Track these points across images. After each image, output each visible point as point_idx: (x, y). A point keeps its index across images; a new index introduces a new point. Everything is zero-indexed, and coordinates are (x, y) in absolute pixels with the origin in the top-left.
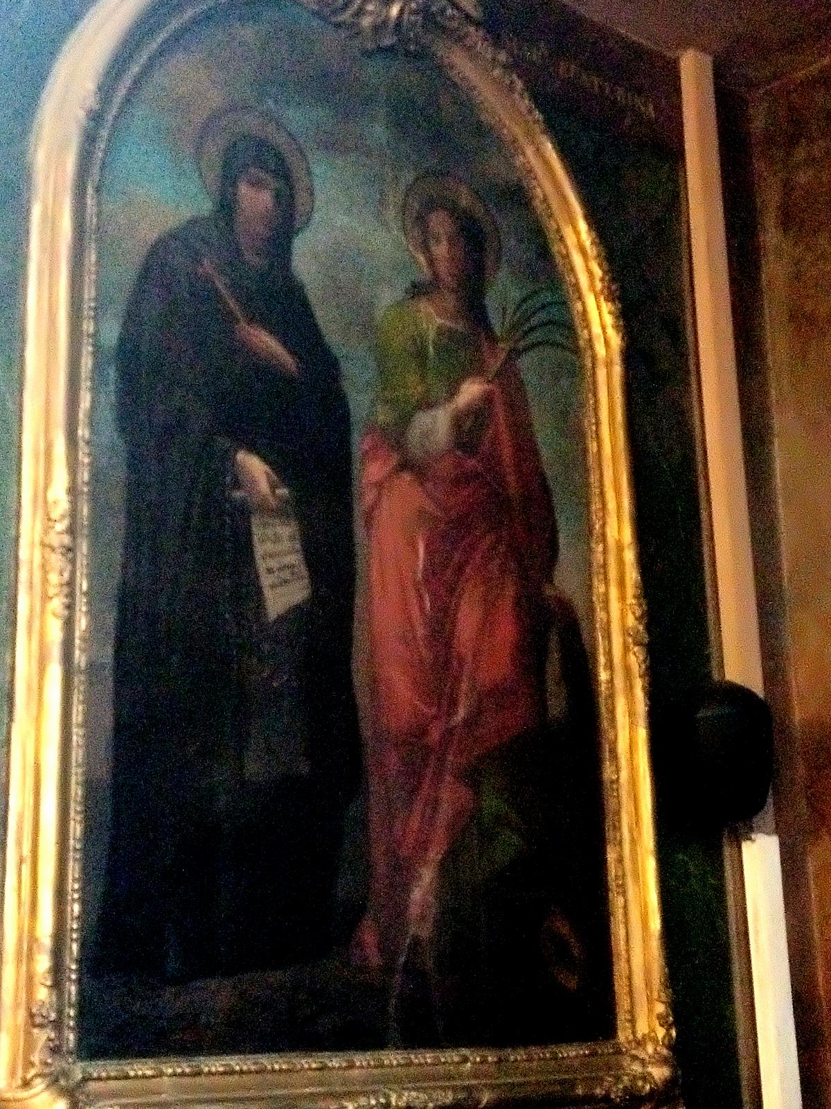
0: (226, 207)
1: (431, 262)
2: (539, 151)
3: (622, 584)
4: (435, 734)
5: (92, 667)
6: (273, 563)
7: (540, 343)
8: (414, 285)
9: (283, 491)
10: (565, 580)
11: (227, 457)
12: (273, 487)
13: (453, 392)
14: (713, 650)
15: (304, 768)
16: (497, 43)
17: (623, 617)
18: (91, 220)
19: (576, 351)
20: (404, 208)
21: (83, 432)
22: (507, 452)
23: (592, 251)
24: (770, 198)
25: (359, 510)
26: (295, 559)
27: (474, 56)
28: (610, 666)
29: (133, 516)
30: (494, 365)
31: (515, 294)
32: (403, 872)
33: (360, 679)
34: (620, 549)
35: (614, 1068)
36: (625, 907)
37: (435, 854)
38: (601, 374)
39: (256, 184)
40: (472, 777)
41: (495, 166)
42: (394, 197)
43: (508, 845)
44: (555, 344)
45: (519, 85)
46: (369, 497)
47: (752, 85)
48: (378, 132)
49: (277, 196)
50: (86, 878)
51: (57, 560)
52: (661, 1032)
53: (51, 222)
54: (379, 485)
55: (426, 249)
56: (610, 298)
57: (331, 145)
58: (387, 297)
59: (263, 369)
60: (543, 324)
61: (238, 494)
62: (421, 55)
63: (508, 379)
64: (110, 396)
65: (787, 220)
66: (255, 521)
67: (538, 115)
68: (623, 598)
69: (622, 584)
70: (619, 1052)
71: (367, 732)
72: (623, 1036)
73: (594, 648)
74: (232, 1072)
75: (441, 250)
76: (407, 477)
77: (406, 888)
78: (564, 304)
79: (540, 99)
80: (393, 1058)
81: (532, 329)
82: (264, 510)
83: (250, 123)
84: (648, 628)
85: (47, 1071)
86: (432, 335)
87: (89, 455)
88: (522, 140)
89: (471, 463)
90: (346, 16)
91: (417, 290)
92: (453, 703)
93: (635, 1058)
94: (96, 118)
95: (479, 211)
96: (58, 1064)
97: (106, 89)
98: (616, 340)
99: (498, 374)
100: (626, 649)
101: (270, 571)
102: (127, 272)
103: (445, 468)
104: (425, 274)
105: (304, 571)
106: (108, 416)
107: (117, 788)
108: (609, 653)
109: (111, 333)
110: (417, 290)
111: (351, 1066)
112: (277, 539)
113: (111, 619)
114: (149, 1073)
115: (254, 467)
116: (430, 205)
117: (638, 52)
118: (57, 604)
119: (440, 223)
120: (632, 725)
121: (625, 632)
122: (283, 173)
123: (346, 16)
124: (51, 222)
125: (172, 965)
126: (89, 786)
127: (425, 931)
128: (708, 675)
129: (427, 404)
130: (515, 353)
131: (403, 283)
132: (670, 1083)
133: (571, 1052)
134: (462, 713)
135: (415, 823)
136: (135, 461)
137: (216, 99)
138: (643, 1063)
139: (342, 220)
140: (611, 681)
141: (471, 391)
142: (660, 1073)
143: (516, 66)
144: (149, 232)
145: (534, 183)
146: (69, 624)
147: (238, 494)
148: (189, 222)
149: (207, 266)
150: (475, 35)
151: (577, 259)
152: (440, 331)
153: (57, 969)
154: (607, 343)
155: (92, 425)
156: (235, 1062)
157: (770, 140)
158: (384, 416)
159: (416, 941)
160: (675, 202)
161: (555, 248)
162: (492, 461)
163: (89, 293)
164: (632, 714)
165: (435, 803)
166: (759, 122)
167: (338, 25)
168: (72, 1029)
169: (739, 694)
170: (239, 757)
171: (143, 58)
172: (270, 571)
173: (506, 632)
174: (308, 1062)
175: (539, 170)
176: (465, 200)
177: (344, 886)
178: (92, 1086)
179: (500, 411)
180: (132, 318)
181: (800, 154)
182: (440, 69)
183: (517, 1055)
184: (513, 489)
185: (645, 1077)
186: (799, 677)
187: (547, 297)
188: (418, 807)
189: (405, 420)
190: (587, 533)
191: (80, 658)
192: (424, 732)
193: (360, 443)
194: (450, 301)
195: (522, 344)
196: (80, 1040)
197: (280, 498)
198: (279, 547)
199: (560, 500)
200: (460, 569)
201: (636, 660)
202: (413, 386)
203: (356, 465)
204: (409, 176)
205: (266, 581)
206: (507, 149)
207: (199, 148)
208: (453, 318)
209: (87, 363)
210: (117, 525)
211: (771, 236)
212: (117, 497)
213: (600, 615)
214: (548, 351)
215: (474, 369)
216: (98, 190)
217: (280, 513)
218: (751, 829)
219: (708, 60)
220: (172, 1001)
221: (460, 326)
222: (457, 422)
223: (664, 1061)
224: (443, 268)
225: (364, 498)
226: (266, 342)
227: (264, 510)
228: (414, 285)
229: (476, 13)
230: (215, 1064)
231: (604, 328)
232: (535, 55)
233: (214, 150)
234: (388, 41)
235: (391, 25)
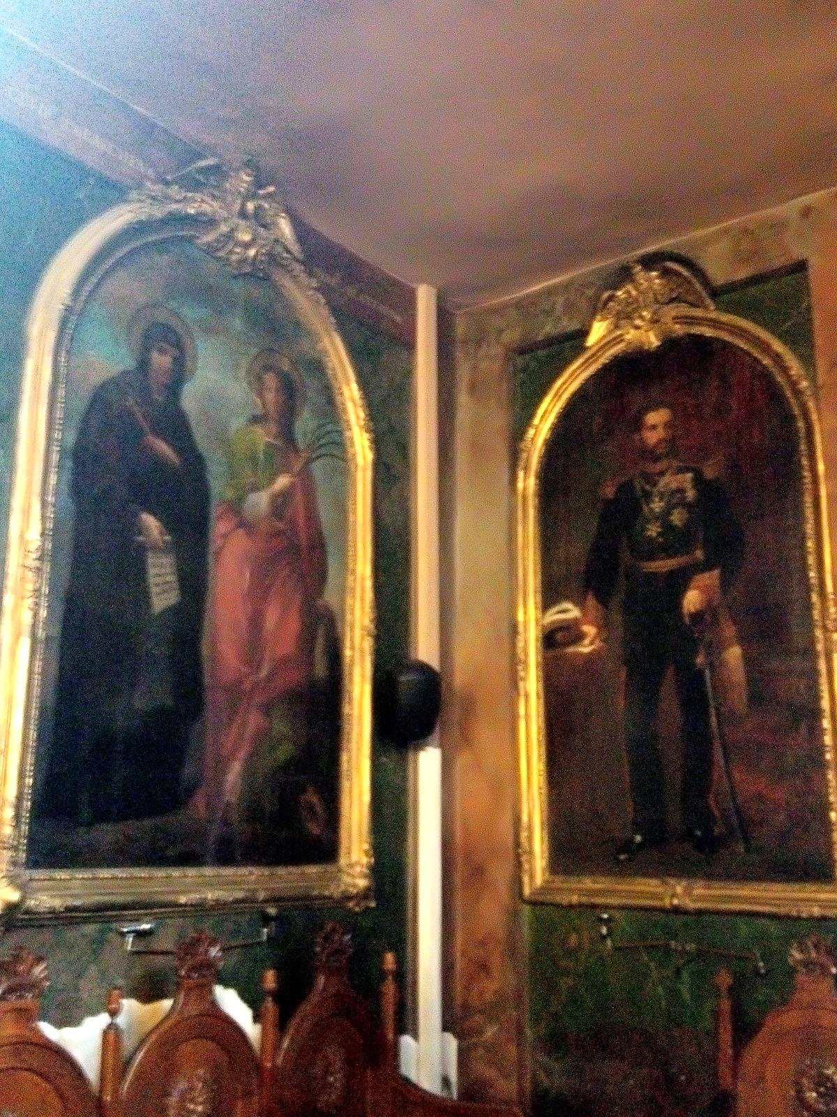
0: (144, 365)
1: (264, 405)
2: (332, 343)
3: (362, 600)
4: (247, 685)
5: (48, 639)
6: (158, 580)
7: (324, 455)
8: (254, 417)
9: (168, 538)
10: (330, 597)
11: (136, 515)
12: (161, 533)
13: (272, 480)
14: (412, 639)
15: (170, 702)
16: (311, 274)
17: (362, 619)
18: (63, 371)
19: (344, 460)
20: (249, 372)
21: (50, 499)
22: (301, 521)
23: (359, 402)
24: (463, 373)
25: (212, 548)
26: (172, 578)
27: (294, 278)
28: (352, 648)
29: (77, 547)
30: (297, 467)
31: (312, 424)
32: (222, 765)
33: (205, 651)
34: (363, 579)
35: (335, 878)
36: (351, 788)
37: (242, 754)
38: (360, 475)
39: (162, 351)
40: (267, 710)
41: (305, 345)
42: (244, 363)
43: (285, 751)
44: (332, 455)
45: (323, 301)
46: (219, 542)
47: (459, 307)
48: (237, 323)
49: (175, 359)
50: (37, 764)
51: (30, 575)
52: (365, 860)
53: (37, 371)
54: (225, 536)
55: (260, 394)
56: (368, 431)
57: (209, 331)
58: (237, 424)
59: (158, 463)
60: (329, 443)
61: (141, 538)
62: (267, 278)
63: (305, 476)
64: (67, 476)
65: (473, 389)
66: (150, 554)
67: (332, 319)
68: (363, 608)
69: (362, 600)
70: (340, 871)
71: (207, 680)
72: (343, 861)
73: (343, 634)
74: (117, 878)
75: (270, 396)
76: (241, 531)
77: (224, 773)
78: (340, 433)
79: (335, 311)
80: (208, 871)
81: (321, 446)
82: (155, 548)
83: (161, 316)
84: (376, 627)
85: (10, 874)
86: (262, 447)
87: (54, 512)
88: (322, 333)
89: (280, 525)
90: (221, 254)
91: (255, 420)
92: (259, 667)
93: (349, 874)
94: (69, 310)
95: (295, 376)
96: (17, 871)
97: (76, 293)
98: (370, 456)
99: (299, 473)
100: (362, 638)
101: (157, 585)
102: (80, 405)
103: (264, 527)
104: (259, 411)
105: (176, 585)
106: (65, 488)
107: (58, 713)
108: (352, 640)
109: (71, 438)
110: (255, 420)
111: (185, 876)
112: (162, 566)
113: (60, 609)
114: (68, 877)
115: (151, 523)
116: (267, 368)
117: (395, 283)
118: (29, 602)
119: (270, 380)
120: (363, 682)
121: (363, 628)
122: (179, 345)
123: (221, 254)
124: (37, 371)
125: (85, 814)
126: (43, 710)
127: (233, 799)
128: (406, 656)
129: (255, 488)
130: (309, 461)
131: (248, 414)
132: (368, 889)
133: (312, 870)
134: (264, 673)
135: (232, 738)
136: (81, 515)
137: (142, 299)
138: (353, 876)
139: (213, 376)
140: (352, 657)
141: (282, 482)
142: (362, 883)
143: (323, 289)
144: (96, 379)
145: (327, 359)
146: (35, 615)
147: (141, 538)
148: (122, 373)
149: (130, 402)
150: (298, 268)
151: (350, 406)
152: (269, 445)
153: (17, 817)
154: (364, 458)
155: (56, 494)
156: (119, 872)
157: (465, 342)
158: (230, 494)
159: (228, 804)
160: (409, 374)
161: (338, 398)
162: (293, 523)
163: (59, 414)
164: (363, 676)
165: (244, 724)
166: (461, 328)
167: (216, 258)
168: (24, 851)
169: (424, 668)
170: (131, 695)
171: (94, 280)
172: (157, 585)
173: (294, 624)
174: (160, 873)
175: (331, 352)
176: (286, 367)
177: (188, 771)
178: (34, 884)
179: (299, 498)
180: (83, 432)
181: (484, 350)
182: (275, 287)
183: (281, 871)
184: (303, 537)
185: (354, 886)
186: (461, 657)
187: (329, 427)
188: (235, 725)
189: (241, 499)
190: (344, 568)
191: (41, 634)
192: (241, 682)
193: (215, 511)
194: (273, 428)
195: (314, 456)
196: (28, 857)
197: (164, 542)
198: (163, 571)
199: (331, 548)
200: (269, 587)
201: (368, 644)
202: (248, 477)
203: (212, 523)
204: (254, 351)
205: (154, 590)
206: (313, 337)
207: (130, 328)
208: (275, 437)
209: (55, 457)
210: (65, 560)
211: (463, 398)
212: (67, 537)
213: (348, 617)
214: (328, 459)
215: (286, 469)
216: (68, 352)
217: (165, 550)
218: (426, 745)
219: (434, 291)
220: (82, 837)
221: (278, 442)
222: (274, 498)
223: (365, 876)
224: (271, 408)
225: (215, 541)
226: (163, 448)
227: (155, 548)
228: (254, 417)
229: (300, 256)
230: (105, 873)
231: (363, 447)
232: (334, 281)
233: (138, 330)
234: (248, 269)
235: (250, 261)
